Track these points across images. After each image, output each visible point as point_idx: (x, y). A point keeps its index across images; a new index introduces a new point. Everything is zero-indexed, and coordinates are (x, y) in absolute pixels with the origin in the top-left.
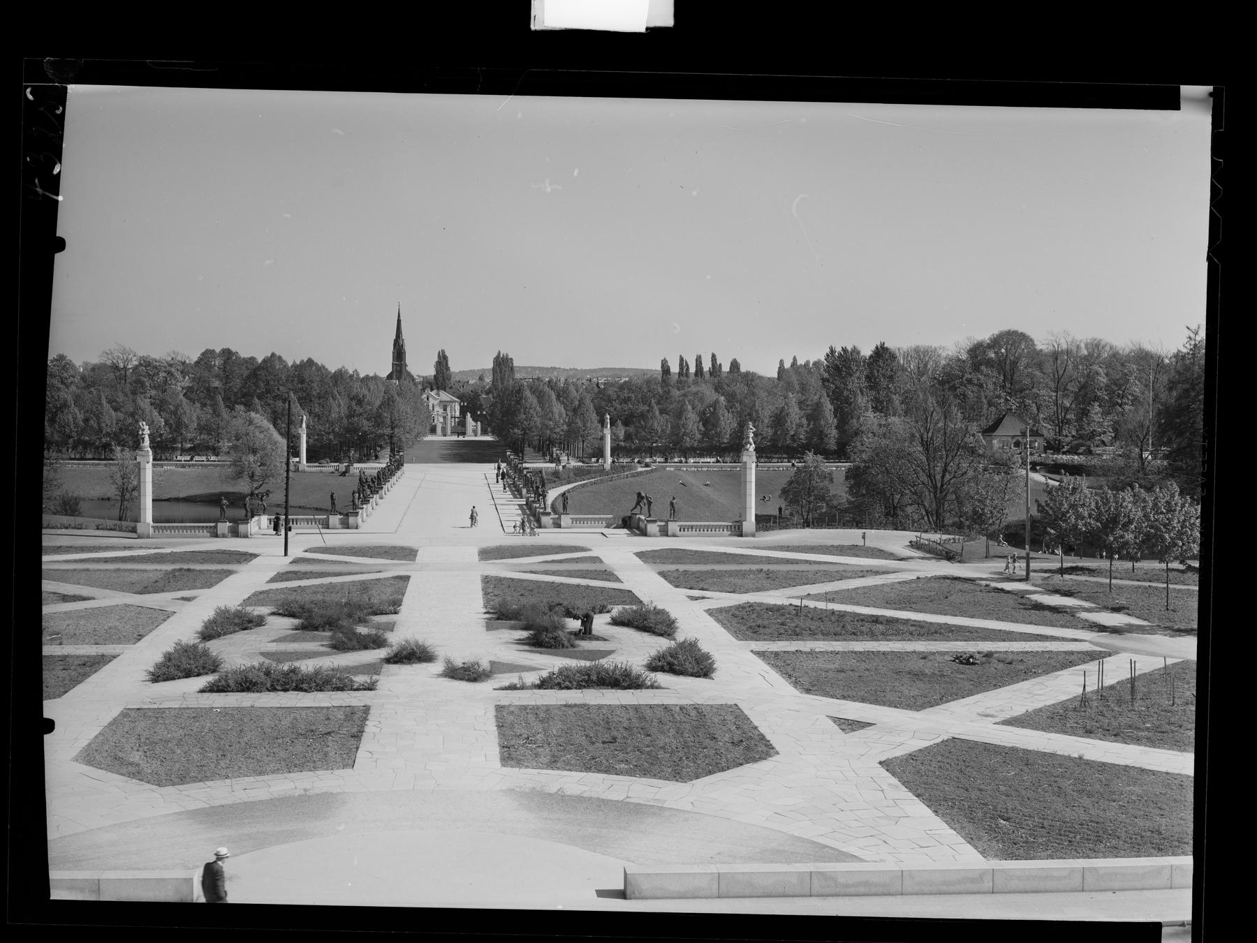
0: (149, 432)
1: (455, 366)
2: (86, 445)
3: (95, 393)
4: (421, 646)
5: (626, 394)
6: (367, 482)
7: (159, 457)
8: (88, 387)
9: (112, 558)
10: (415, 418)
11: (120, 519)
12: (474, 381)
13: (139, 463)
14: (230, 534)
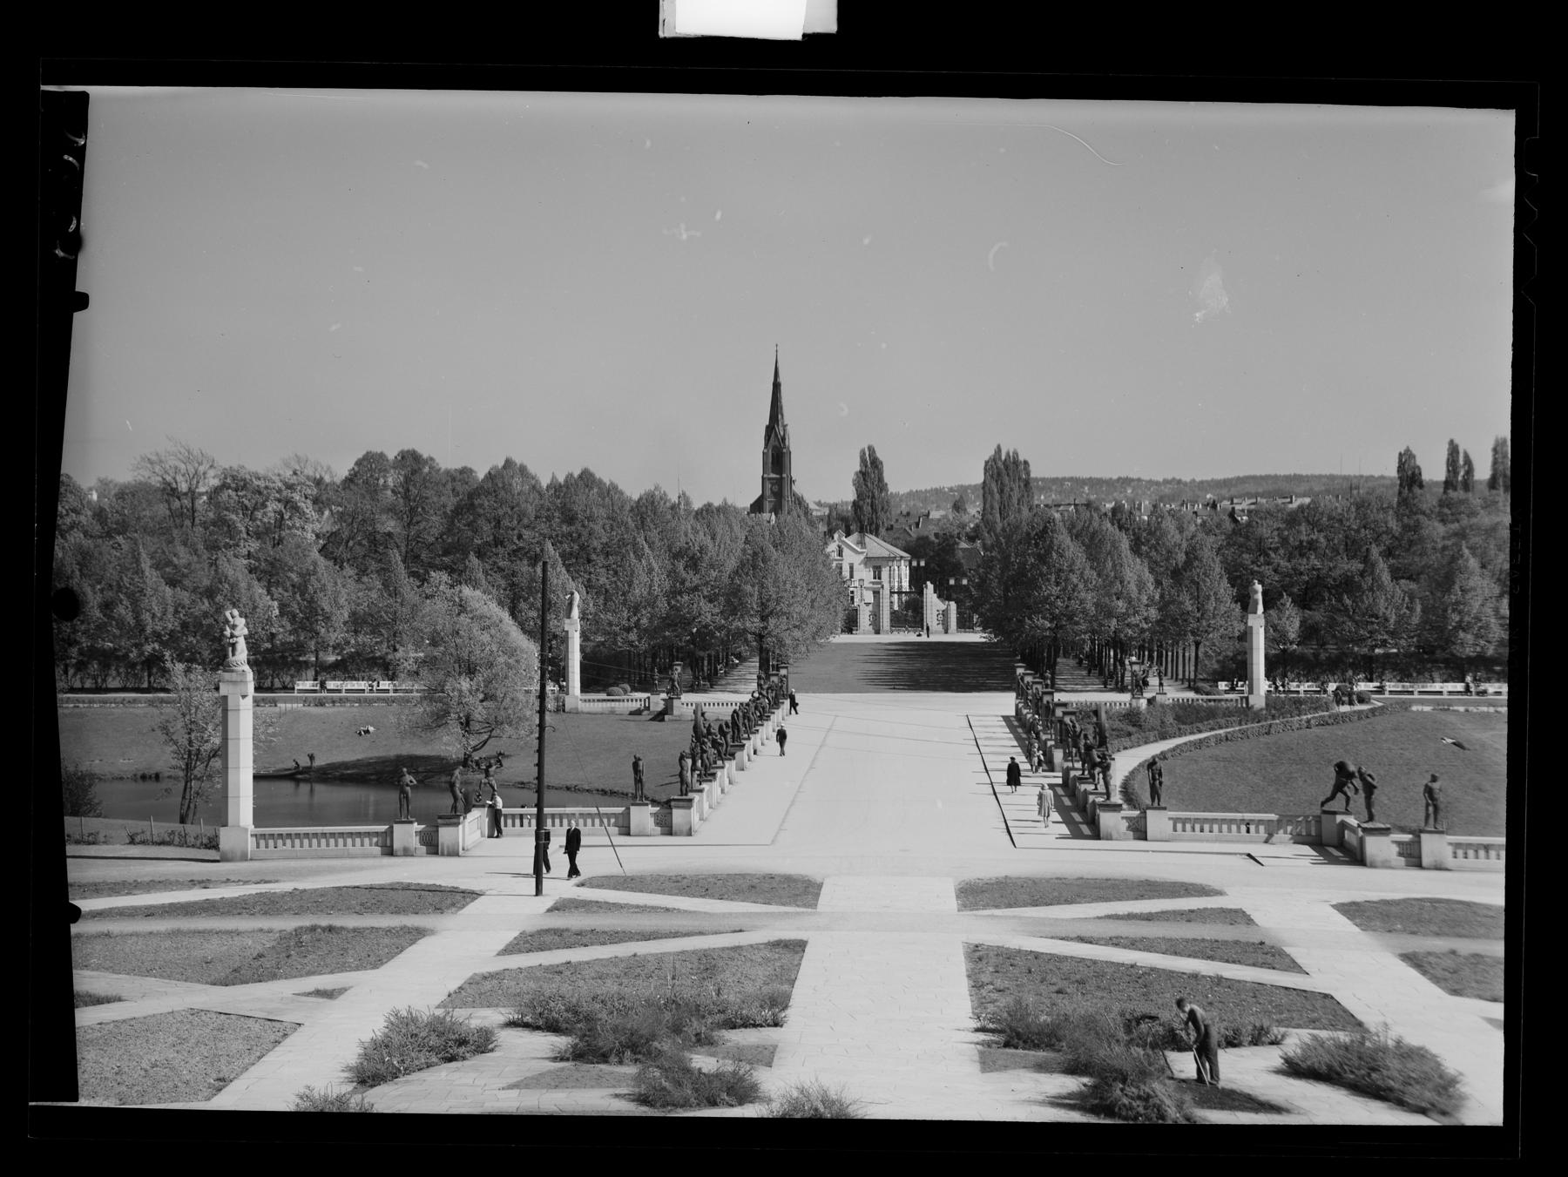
0: (246, 631)
1: (899, 481)
3: (125, 547)
4: (833, 1102)
5: (1304, 533)
6: (709, 733)
7: (268, 683)
8: (109, 535)
9: (163, 906)
10: (811, 595)
12: (942, 513)
13: (225, 698)
14: (424, 848)
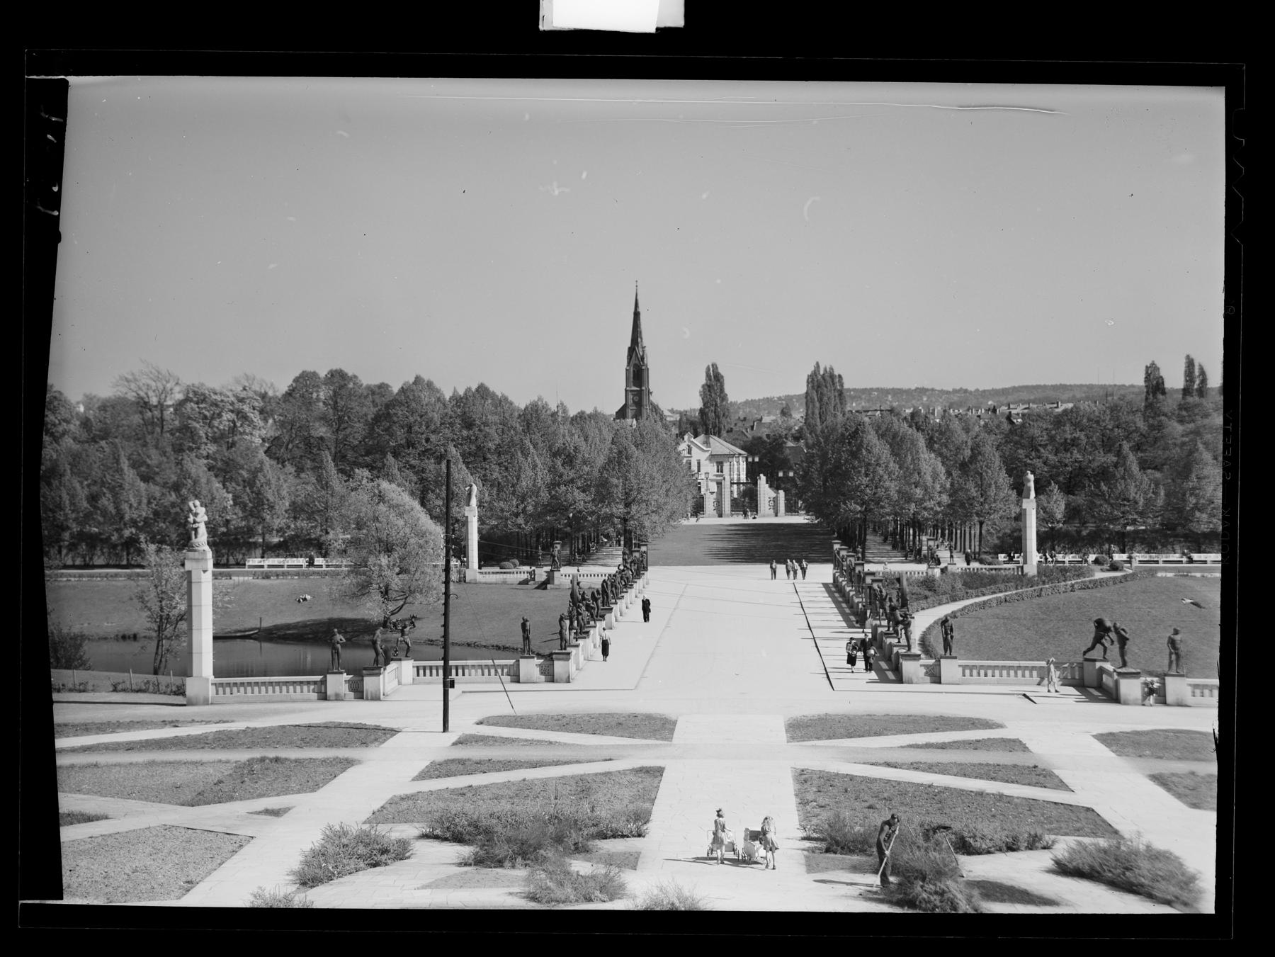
0: (206, 518)
1: (737, 392)
2: (93, 541)
4: (687, 899)
5: (1068, 432)
6: (584, 599)
7: (224, 561)
8: (94, 440)
9: (141, 742)
11: (156, 673)
12: (773, 418)
